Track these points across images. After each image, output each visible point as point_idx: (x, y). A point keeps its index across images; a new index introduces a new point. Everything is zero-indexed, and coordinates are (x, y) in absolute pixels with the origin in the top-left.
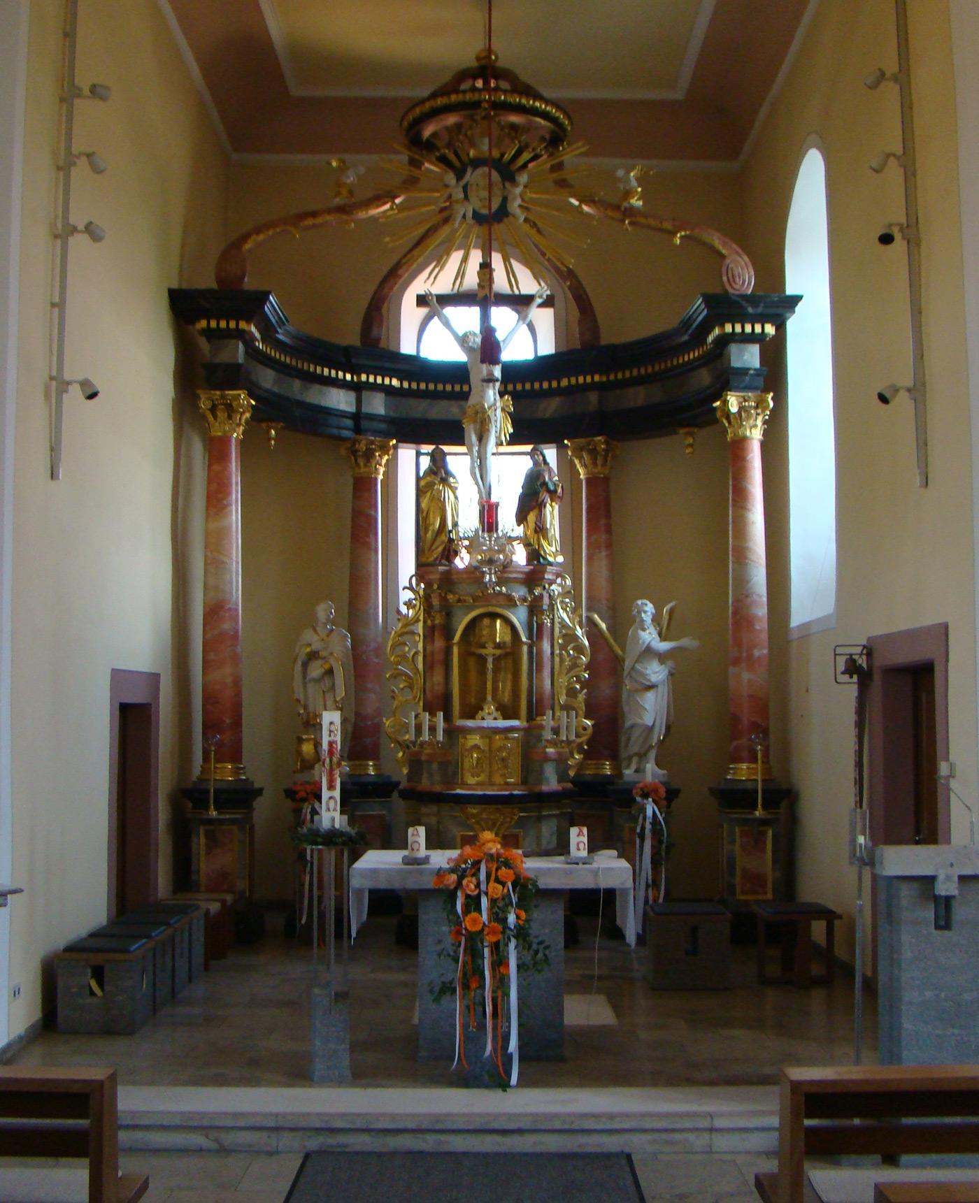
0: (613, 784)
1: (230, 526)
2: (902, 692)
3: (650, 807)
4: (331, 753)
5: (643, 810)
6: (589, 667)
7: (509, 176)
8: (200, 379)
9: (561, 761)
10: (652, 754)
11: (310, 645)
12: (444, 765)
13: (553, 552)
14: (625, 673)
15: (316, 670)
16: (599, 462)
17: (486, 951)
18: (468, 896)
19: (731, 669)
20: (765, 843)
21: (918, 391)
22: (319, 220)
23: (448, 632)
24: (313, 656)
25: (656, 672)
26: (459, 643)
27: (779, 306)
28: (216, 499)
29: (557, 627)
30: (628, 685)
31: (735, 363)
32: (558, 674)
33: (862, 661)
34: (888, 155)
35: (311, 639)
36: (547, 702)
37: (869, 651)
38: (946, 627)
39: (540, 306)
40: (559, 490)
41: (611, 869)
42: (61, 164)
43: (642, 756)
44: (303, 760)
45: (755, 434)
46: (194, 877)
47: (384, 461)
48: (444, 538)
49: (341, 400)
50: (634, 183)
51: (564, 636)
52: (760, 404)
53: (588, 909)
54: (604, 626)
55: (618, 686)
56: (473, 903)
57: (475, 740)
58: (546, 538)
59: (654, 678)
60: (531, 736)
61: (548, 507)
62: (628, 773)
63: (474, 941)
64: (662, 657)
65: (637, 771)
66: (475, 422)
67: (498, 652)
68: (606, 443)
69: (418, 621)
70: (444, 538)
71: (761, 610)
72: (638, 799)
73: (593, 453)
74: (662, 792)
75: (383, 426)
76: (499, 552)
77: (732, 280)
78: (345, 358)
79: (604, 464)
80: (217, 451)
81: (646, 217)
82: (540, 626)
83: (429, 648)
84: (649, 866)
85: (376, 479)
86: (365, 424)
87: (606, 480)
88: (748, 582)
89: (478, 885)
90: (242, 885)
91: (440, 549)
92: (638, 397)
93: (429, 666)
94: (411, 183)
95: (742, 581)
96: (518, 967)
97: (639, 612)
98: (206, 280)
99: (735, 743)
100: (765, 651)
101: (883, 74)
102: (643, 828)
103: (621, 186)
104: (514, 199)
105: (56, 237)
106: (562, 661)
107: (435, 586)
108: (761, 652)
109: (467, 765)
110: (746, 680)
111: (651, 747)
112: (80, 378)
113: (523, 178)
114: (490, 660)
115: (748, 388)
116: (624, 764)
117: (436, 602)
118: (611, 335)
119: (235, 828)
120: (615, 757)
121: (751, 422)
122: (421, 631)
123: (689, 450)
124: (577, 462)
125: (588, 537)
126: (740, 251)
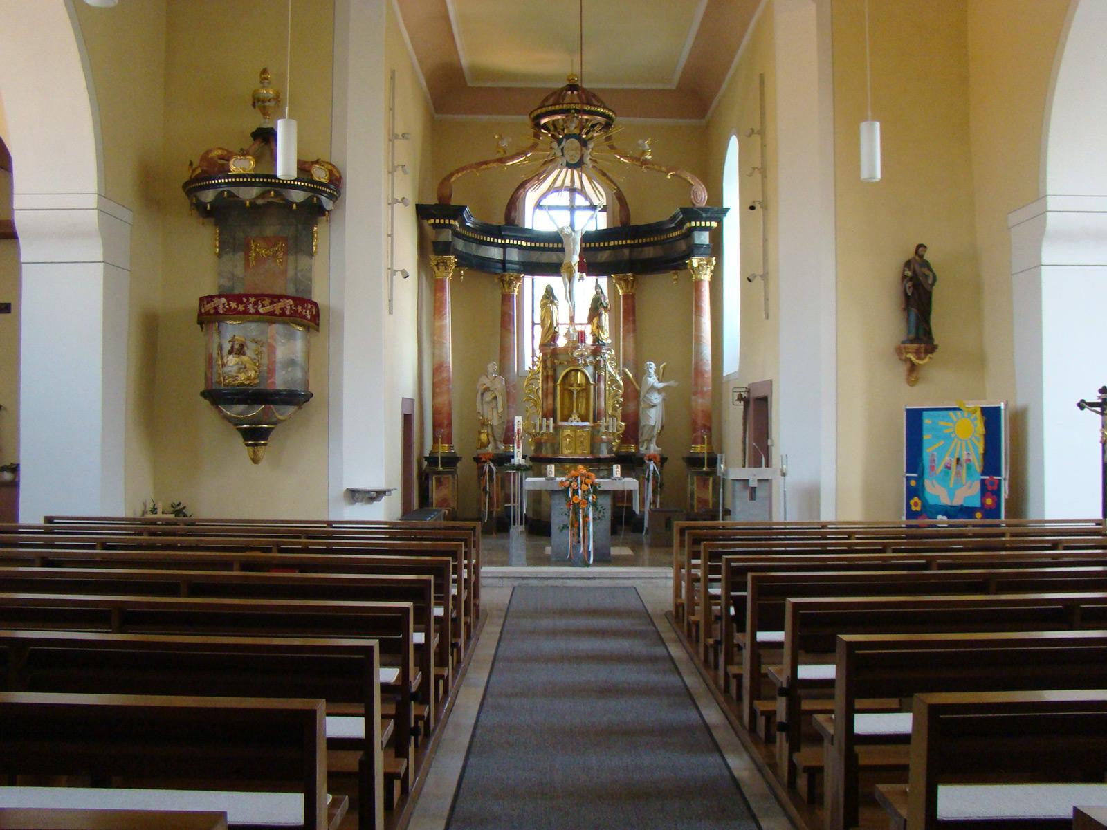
0: (634, 456)
1: (446, 325)
2: (758, 406)
3: (652, 466)
4: (518, 434)
5: (649, 467)
6: (623, 396)
7: (584, 143)
8: (431, 249)
9: (609, 443)
10: (654, 440)
11: (485, 384)
12: (553, 445)
13: (606, 337)
14: (641, 399)
15: (488, 397)
16: (630, 286)
17: (581, 511)
18: (574, 490)
19: (693, 397)
20: (708, 485)
21: (765, 277)
22: (489, 166)
23: (555, 380)
24: (487, 390)
25: (656, 398)
26: (560, 385)
27: (719, 213)
28: (438, 311)
29: (608, 375)
30: (643, 405)
31: (697, 242)
32: (608, 399)
33: (745, 395)
34: (754, 168)
35: (485, 381)
36: (603, 412)
37: (748, 391)
38: (771, 381)
39: (600, 211)
40: (609, 307)
41: (631, 483)
42: (390, 170)
43: (649, 441)
44: (482, 443)
45: (706, 277)
46: (430, 501)
47: (517, 286)
48: (552, 331)
49: (496, 253)
50: (648, 147)
51: (611, 380)
52: (709, 262)
53: (621, 499)
54: (630, 375)
55: (638, 405)
56: (576, 492)
57: (568, 432)
58: (602, 331)
59: (655, 402)
60: (595, 430)
61: (603, 316)
62: (642, 449)
63: (576, 507)
64: (659, 391)
65: (646, 448)
66: (567, 272)
67: (579, 388)
68: (634, 276)
69: (539, 372)
70: (552, 331)
71: (708, 367)
72: (646, 461)
73: (626, 281)
74: (658, 459)
75: (517, 266)
76: (585, 351)
77: (696, 198)
78: (497, 232)
79: (632, 287)
80: (437, 287)
81: (653, 165)
82: (599, 376)
83: (545, 387)
84: (651, 494)
85: (513, 295)
86: (508, 265)
87: (633, 296)
88: (701, 353)
89: (577, 486)
90: (454, 504)
91: (550, 337)
92: (649, 253)
93: (545, 395)
94: (533, 147)
95: (699, 352)
96: (593, 519)
97: (648, 368)
98: (433, 200)
99: (695, 435)
100: (710, 388)
101: (753, 130)
102: (649, 475)
103: (641, 148)
104: (587, 156)
105: (389, 204)
106: (610, 393)
107: (549, 356)
108: (708, 388)
109: (564, 444)
110: (701, 403)
111: (654, 436)
112: (402, 269)
113: (591, 145)
114: (575, 392)
115: (703, 254)
116: (640, 445)
117: (549, 364)
118: (635, 221)
119: (450, 476)
120: (637, 443)
121: (704, 272)
122: (540, 378)
123: (675, 282)
124: (618, 286)
125: (624, 327)
126: (700, 182)
